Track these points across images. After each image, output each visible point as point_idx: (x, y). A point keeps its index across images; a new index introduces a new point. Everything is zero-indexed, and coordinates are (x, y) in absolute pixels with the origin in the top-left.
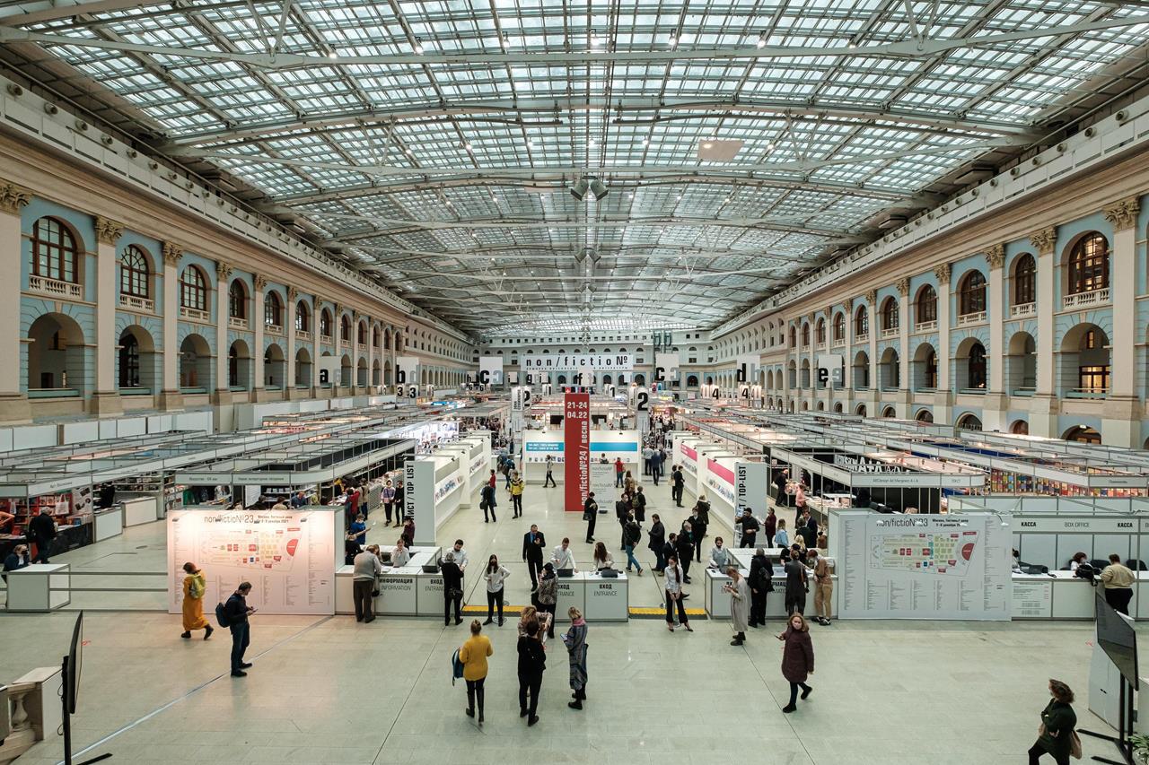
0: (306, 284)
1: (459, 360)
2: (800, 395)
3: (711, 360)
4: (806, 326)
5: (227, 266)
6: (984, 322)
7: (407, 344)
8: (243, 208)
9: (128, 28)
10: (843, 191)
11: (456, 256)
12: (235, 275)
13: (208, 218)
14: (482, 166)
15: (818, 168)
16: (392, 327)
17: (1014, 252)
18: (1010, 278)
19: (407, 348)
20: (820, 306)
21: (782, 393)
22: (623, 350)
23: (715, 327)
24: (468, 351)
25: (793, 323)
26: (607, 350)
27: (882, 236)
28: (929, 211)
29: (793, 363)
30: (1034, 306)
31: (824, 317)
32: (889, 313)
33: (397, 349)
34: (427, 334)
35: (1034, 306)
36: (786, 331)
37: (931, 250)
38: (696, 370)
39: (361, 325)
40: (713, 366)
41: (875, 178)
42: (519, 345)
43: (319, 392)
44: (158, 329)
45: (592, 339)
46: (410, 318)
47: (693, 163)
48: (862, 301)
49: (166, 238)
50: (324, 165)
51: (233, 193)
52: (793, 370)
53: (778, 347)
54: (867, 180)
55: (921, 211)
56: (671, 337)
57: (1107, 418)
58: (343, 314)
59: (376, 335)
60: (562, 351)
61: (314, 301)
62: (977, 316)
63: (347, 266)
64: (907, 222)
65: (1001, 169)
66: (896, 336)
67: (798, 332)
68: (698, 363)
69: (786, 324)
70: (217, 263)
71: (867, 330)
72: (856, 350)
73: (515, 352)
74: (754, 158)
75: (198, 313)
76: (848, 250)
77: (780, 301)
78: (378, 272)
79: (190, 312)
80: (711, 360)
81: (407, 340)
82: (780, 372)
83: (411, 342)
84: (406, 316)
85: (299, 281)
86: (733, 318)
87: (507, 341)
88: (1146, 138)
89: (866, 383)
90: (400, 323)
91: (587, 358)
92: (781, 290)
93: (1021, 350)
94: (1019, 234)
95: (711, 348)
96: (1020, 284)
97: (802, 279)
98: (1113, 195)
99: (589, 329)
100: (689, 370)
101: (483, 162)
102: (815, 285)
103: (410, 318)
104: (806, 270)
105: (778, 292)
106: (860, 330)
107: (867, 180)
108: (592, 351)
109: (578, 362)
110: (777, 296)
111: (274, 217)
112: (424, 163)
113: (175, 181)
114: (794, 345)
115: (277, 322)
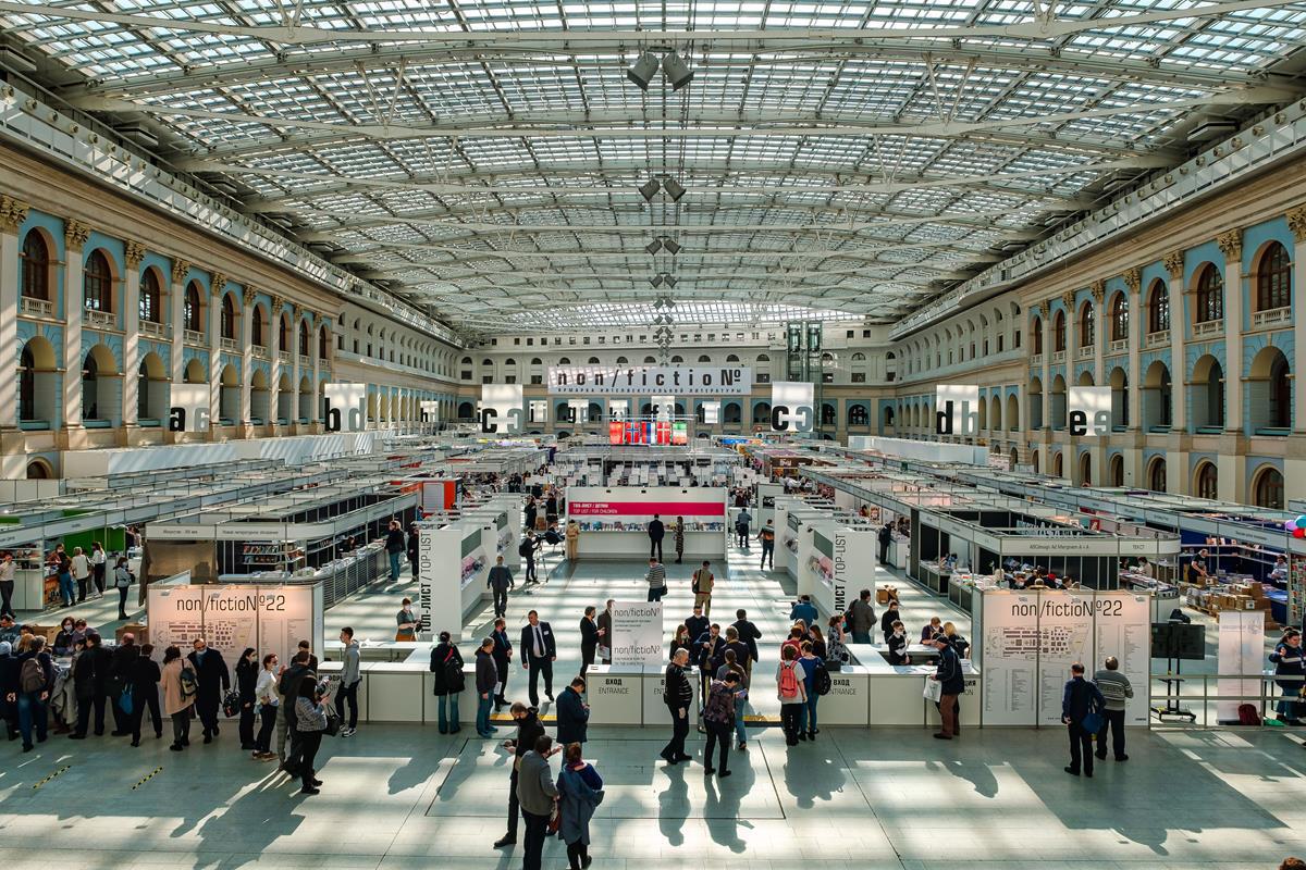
0: (159, 238)
1: (439, 377)
2: (1049, 440)
3: (891, 376)
4: (1061, 316)
5: (20, 205)
6: (1288, 322)
7: (340, 347)
8: (48, 101)
9: (183, 40)
10: (1124, 73)
11: (429, 187)
12: (95, 243)
13: (149, 199)
14: (475, 26)
15: (1078, 33)
16: (314, 315)
17: (1195, 262)
18: (1031, 334)
19: (341, 353)
20: (1084, 278)
21: (1019, 438)
22: (733, 358)
23: (899, 317)
24: (453, 358)
25: (1037, 311)
26: (705, 359)
27: (1194, 154)
28: (1278, 109)
29: (1037, 381)
30: (1168, 334)
31: (1092, 299)
32: (1207, 286)
33: (323, 355)
34: (376, 330)
35: (1221, 323)
36: (1024, 324)
37: (1282, 180)
38: (865, 394)
39: (257, 312)
40: (896, 387)
41: (1181, 51)
42: (544, 349)
43: (299, 428)
44: (166, 356)
45: (677, 337)
46: (347, 300)
47: (855, 23)
48: (1158, 271)
49: (68, 213)
50: (196, 26)
51: (30, 74)
52: (1036, 396)
53: (1010, 353)
54: (1165, 55)
55: (1264, 109)
56: (818, 333)
57: (1291, 457)
58: (255, 302)
59: (305, 336)
60: (622, 360)
61: (244, 293)
62: (1213, 325)
63: (233, 205)
64: (1238, 130)
65: (1243, 126)
66: (1218, 333)
67: (1045, 325)
68: (868, 382)
69: (1025, 313)
70: (65, 223)
71: (1166, 326)
72: (1149, 360)
73: (537, 361)
74: (962, 15)
75: (103, 316)
76: (1136, 180)
77: (1014, 272)
78: (288, 216)
79: (94, 315)
80: (891, 376)
81: (340, 338)
82: (1013, 398)
83: (349, 344)
84: (339, 296)
85: (146, 232)
86: (931, 300)
87: (524, 340)
88: (1303, 144)
89: (1166, 418)
90: (326, 307)
91: (669, 372)
92: (1018, 251)
93: (1157, 382)
94: (1202, 237)
95: (891, 356)
96: (1204, 300)
97: (1052, 232)
98: (1251, 215)
99: (670, 321)
100: (852, 394)
101: (478, 20)
102: (1074, 243)
103: (347, 300)
104: (1061, 214)
105: (1009, 254)
106: (1157, 323)
107: (1165, 55)
108: (677, 359)
109: (651, 380)
110: (1009, 262)
111: (105, 117)
112: (371, 21)
113: (34, 112)
114: (1039, 350)
115: (107, 306)
